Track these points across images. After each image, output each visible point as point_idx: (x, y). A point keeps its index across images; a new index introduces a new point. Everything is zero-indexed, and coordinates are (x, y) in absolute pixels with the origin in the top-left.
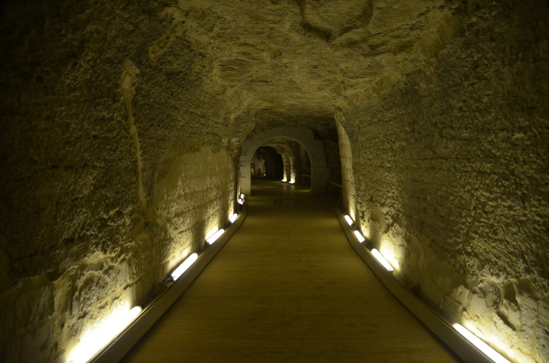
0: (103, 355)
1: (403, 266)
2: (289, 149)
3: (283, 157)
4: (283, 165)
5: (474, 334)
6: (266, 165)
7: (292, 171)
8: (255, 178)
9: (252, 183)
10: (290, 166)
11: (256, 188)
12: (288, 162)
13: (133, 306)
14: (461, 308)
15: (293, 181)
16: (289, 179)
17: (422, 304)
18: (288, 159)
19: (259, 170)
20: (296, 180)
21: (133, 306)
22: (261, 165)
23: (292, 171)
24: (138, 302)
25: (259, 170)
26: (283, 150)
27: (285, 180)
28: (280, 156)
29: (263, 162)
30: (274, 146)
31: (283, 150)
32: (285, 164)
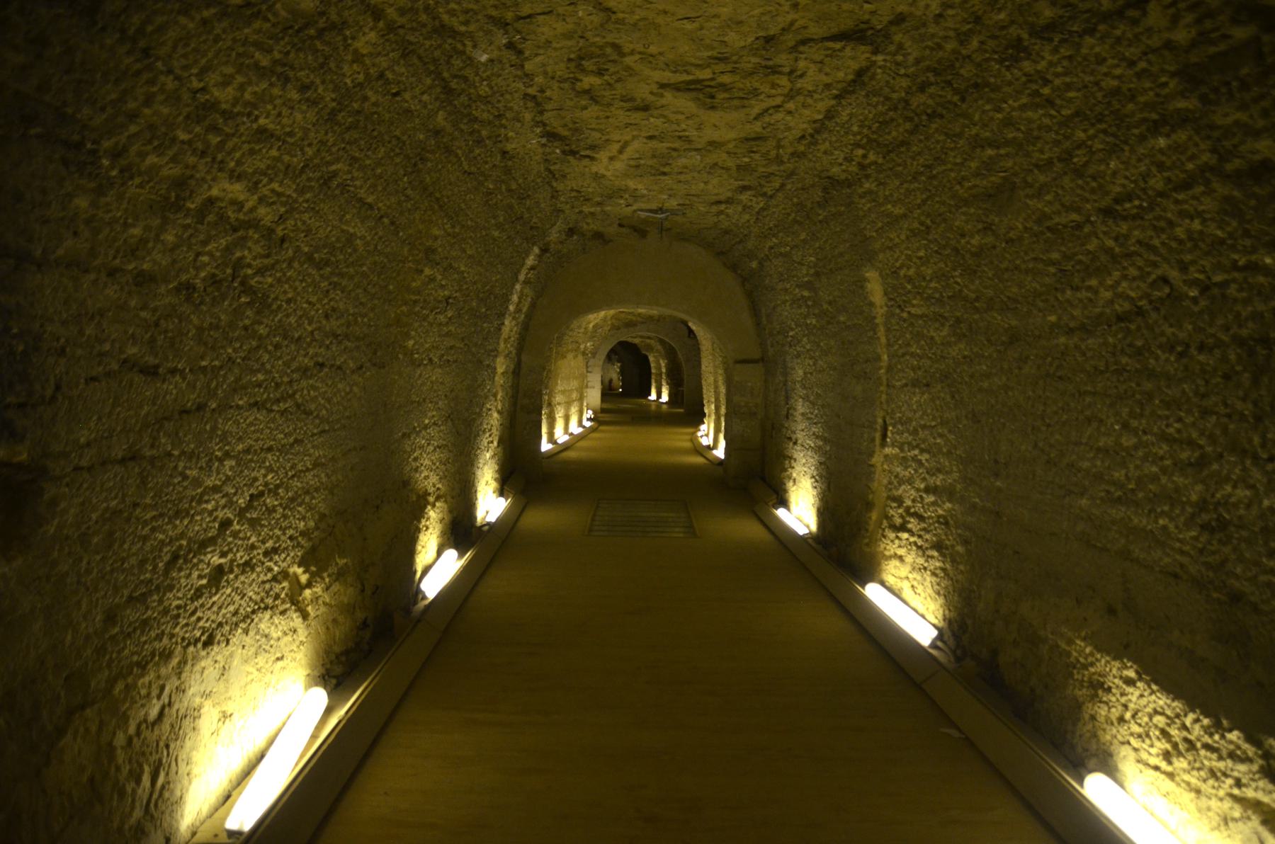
0: (276, 816)
1: (821, 524)
2: (659, 347)
3: (651, 359)
4: (650, 373)
5: (280, 730)
6: (622, 372)
7: (664, 383)
8: (608, 392)
9: (603, 401)
10: (661, 374)
11: (605, 406)
12: (659, 368)
13: (308, 686)
14: (874, 516)
15: (665, 398)
16: (659, 396)
17: (1009, 718)
18: (658, 364)
19: (611, 381)
20: (670, 396)
21: (308, 686)
22: (614, 373)
23: (664, 383)
24: (335, 672)
25: (611, 381)
26: (650, 348)
27: (653, 396)
28: (646, 358)
29: (617, 367)
30: (637, 341)
31: (650, 348)
32: (653, 371)
